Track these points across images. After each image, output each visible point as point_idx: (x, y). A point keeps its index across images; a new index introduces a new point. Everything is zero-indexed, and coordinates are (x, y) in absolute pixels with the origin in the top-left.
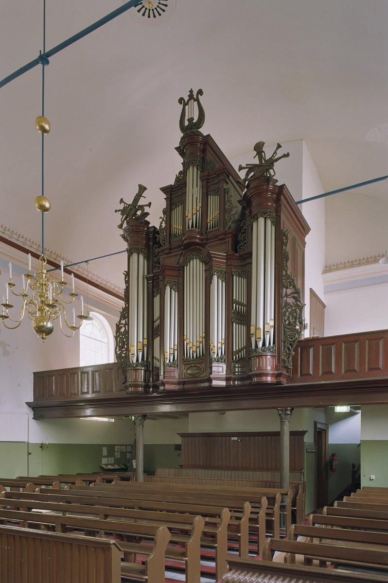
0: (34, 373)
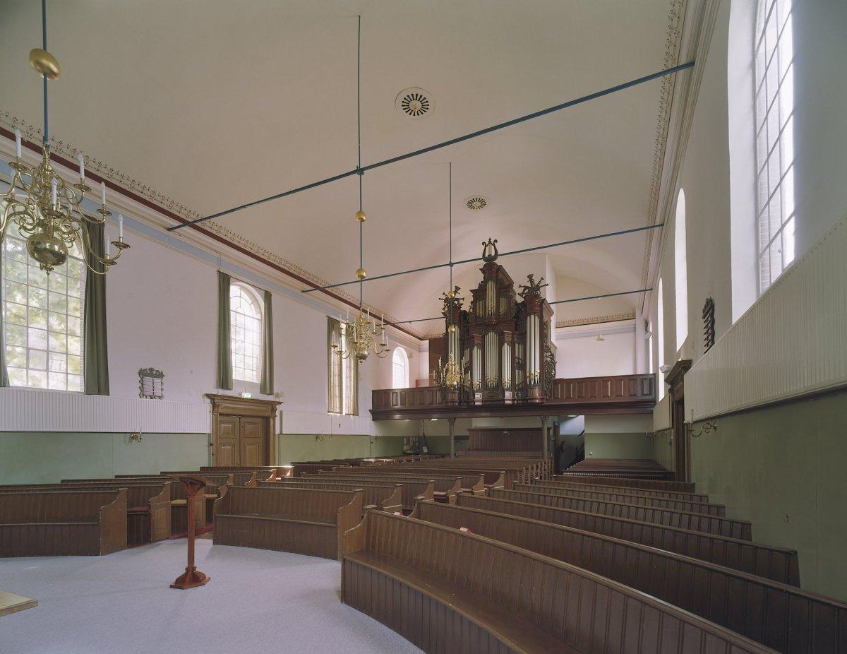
0: (373, 391)
